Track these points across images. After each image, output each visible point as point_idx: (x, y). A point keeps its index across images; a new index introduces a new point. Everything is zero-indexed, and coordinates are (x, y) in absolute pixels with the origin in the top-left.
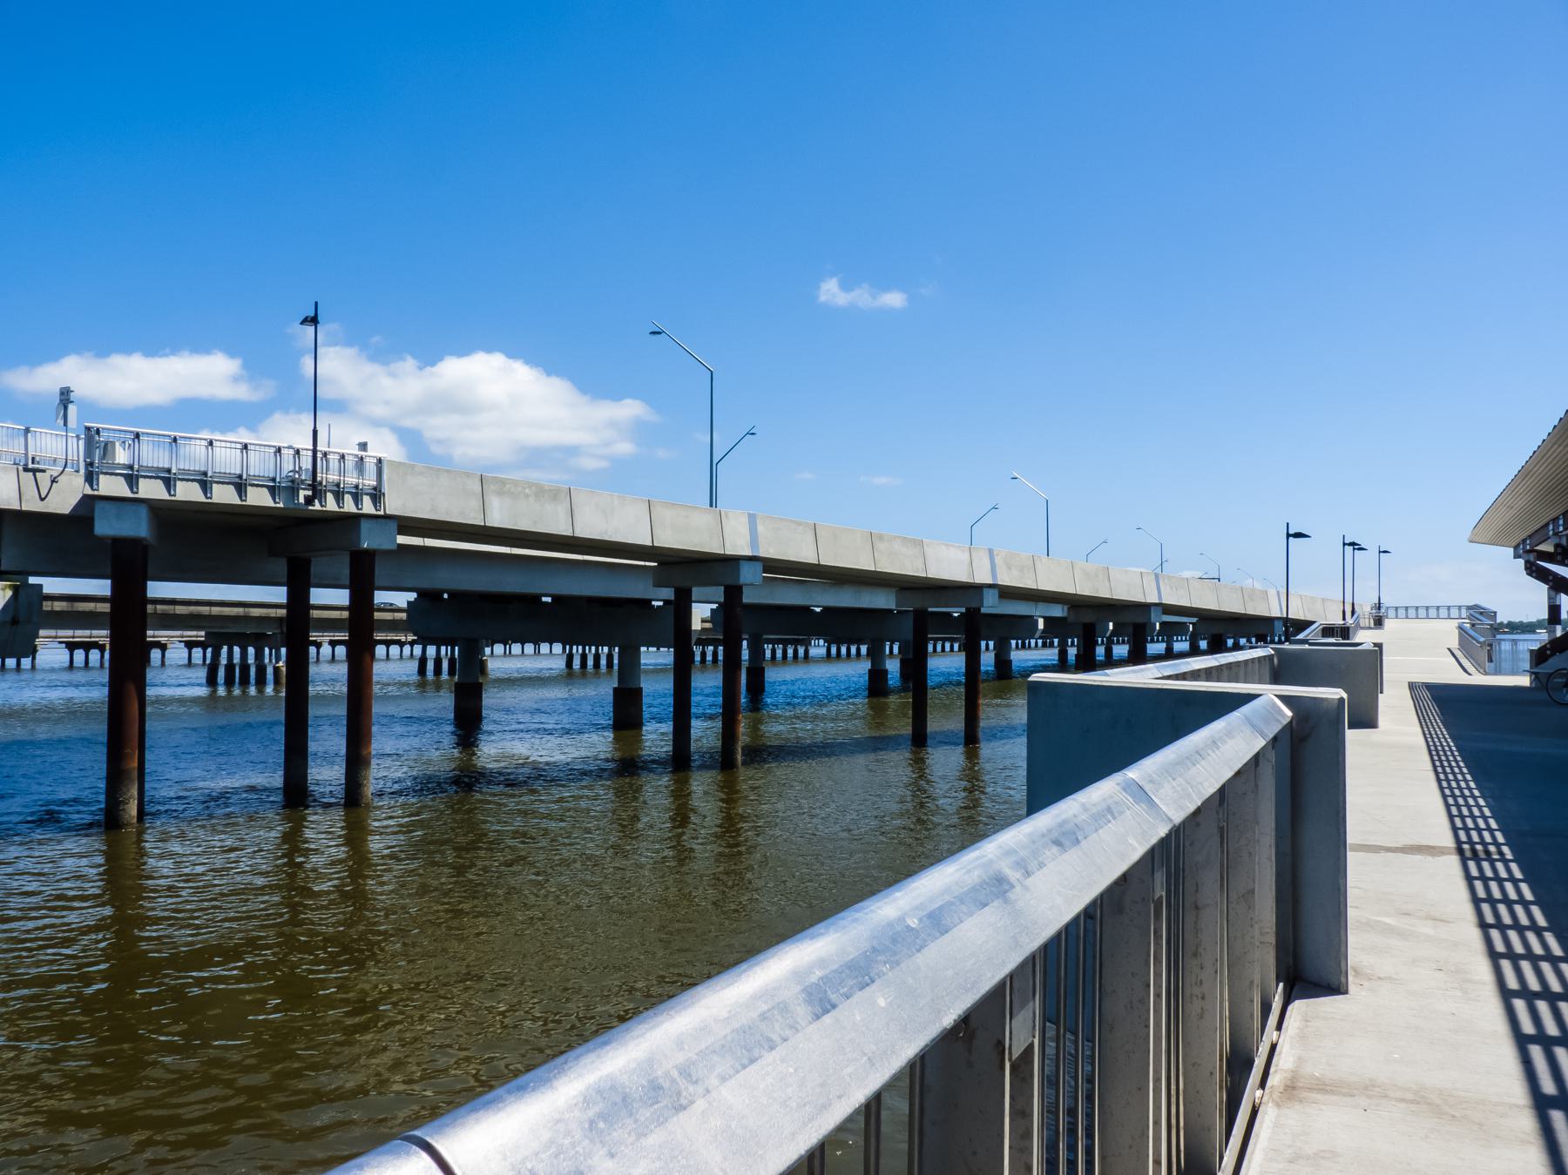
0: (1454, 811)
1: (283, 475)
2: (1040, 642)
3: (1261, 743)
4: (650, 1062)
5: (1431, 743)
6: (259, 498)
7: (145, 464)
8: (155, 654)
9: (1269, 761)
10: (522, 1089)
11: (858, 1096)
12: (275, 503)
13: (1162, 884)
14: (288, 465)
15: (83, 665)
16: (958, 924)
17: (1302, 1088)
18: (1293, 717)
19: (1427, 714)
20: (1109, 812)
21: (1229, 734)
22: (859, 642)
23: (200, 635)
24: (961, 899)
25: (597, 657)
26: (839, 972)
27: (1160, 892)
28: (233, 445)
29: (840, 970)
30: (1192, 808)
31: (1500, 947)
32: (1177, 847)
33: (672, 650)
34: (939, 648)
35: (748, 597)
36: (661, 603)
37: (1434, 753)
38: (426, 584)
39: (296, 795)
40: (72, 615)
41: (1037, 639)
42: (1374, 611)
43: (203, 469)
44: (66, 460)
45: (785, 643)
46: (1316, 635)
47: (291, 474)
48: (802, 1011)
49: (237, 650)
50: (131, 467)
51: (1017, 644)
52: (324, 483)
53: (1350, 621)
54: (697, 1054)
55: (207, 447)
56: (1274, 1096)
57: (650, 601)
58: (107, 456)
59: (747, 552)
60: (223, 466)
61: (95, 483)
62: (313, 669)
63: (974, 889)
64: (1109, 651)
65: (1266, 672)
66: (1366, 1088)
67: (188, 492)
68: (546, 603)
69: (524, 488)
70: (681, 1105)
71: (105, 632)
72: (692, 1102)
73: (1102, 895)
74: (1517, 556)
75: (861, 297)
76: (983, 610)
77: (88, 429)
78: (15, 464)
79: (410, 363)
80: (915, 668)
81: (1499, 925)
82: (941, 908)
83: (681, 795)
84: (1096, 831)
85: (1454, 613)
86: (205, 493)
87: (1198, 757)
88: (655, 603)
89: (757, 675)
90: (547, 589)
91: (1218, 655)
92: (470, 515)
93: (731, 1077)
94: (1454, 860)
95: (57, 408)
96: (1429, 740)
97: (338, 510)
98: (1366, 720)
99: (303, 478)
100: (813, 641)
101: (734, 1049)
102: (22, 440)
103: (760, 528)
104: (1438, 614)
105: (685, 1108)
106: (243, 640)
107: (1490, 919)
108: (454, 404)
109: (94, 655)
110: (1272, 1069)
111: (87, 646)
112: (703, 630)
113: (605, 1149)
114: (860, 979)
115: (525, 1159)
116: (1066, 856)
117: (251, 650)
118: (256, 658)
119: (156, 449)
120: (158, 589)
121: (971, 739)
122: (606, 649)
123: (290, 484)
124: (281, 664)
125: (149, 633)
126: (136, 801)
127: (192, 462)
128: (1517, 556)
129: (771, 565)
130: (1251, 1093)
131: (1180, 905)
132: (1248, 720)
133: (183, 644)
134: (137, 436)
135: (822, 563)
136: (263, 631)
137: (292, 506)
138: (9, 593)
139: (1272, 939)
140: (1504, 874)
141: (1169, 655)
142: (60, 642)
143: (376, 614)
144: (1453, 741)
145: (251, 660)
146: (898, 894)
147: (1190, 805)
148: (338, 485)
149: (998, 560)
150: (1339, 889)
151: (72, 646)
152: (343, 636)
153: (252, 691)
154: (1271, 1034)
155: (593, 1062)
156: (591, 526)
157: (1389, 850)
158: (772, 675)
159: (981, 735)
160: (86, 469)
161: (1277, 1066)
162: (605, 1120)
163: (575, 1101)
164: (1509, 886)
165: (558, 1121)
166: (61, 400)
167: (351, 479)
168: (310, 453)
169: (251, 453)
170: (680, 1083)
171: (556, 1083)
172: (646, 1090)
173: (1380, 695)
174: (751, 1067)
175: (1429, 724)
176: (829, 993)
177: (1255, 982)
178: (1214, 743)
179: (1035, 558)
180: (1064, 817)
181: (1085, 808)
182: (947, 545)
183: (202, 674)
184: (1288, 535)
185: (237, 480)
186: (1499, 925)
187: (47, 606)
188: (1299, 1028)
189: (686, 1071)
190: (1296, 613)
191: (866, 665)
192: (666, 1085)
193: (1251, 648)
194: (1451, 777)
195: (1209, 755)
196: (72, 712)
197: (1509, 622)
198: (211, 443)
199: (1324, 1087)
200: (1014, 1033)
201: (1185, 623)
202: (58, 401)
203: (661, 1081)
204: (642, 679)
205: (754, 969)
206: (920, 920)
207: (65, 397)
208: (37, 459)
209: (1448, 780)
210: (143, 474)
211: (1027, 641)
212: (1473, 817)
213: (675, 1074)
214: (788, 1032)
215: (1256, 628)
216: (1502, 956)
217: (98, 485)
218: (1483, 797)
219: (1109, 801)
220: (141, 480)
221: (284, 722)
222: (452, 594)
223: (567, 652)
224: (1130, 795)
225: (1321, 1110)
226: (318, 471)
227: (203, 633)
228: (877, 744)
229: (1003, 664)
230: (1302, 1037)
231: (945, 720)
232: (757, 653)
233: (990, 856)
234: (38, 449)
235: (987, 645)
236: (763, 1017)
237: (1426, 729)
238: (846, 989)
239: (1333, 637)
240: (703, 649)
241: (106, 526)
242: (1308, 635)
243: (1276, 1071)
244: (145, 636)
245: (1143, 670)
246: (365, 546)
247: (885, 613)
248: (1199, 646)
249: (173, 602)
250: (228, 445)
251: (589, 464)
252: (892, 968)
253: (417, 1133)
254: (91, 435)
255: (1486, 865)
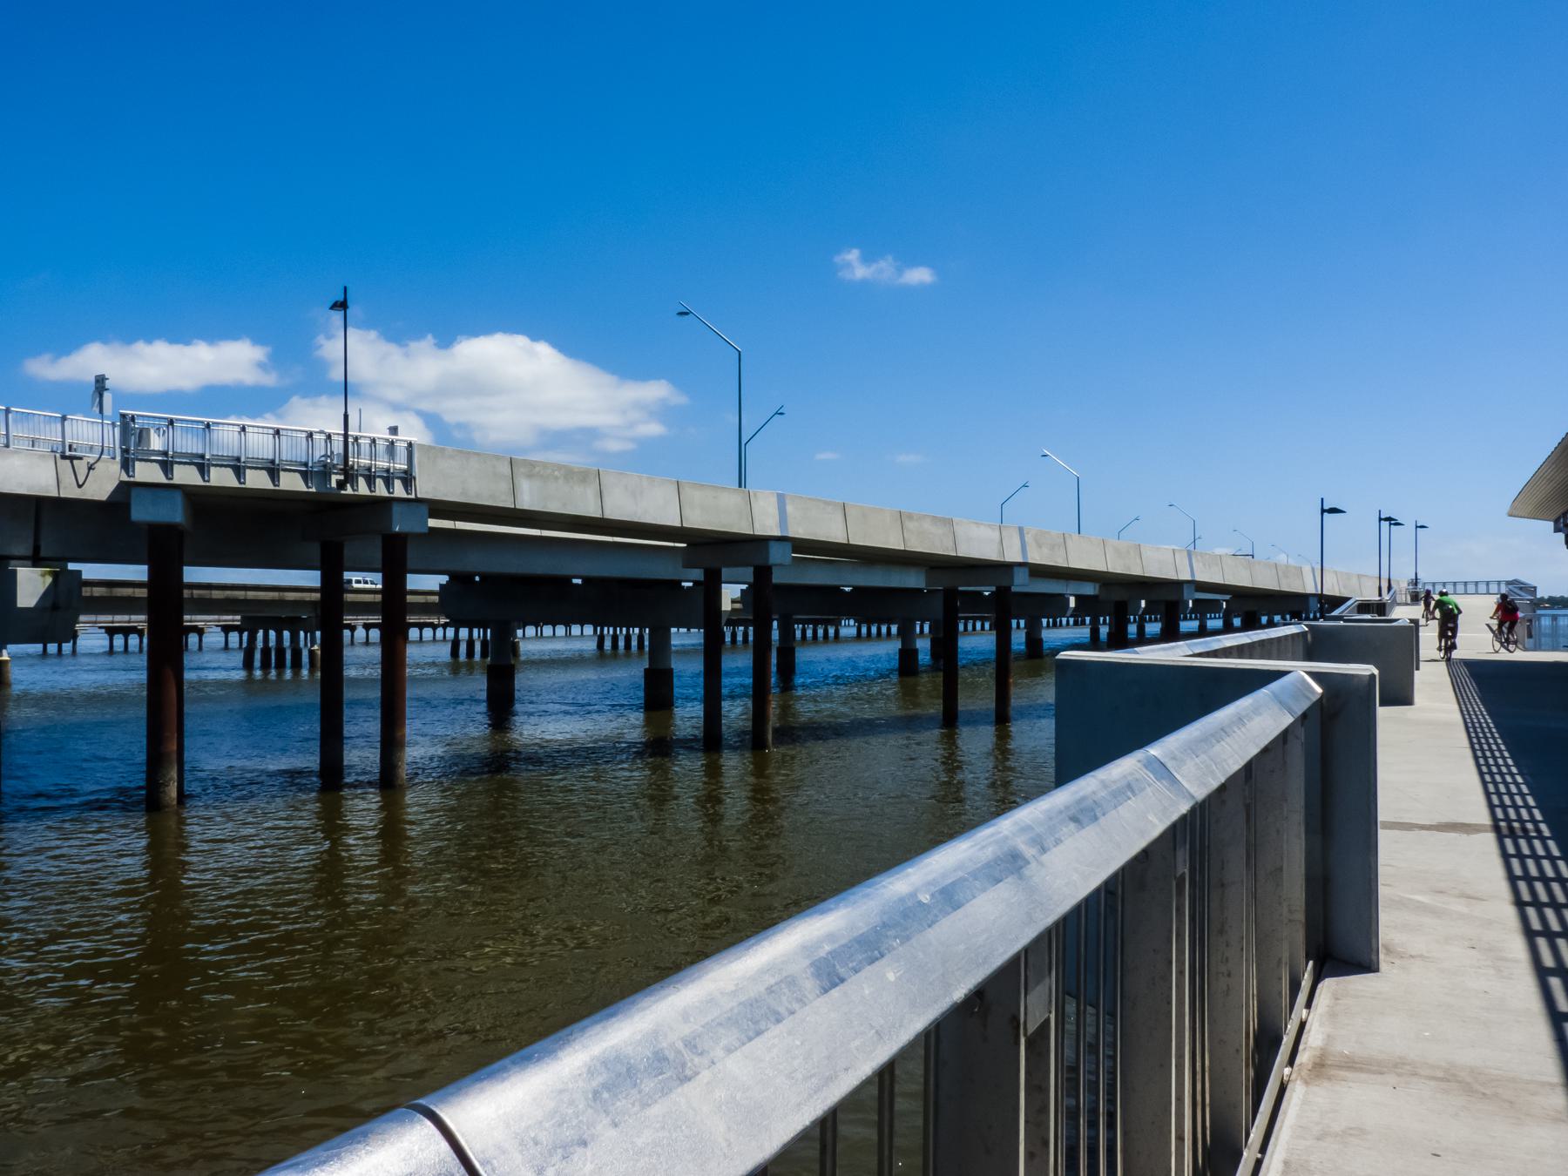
0: (1491, 788)
1: (316, 459)
2: (1071, 620)
3: (1288, 720)
4: (655, 1034)
5: (1468, 720)
6: (291, 482)
7: (179, 451)
8: (193, 639)
9: (1297, 738)
10: (528, 1059)
11: (866, 1067)
12: (308, 487)
13: (1185, 861)
14: (319, 452)
15: (122, 649)
16: (971, 900)
17: (1330, 1065)
18: (1323, 694)
19: (1464, 688)
20: (1129, 789)
21: (1256, 710)
22: (889, 622)
23: (235, 619)
24: (975, 875)
25: (628, 638)
26: (847, 946)
27: (1183, 869)
28: (265, 431)
29: (850, 945)
30: (1215, 784)
31: (1536, 925)
32: (1202, 825)
33: (702, 630)
34: (970, 627)
35: (778, 578)
36: (691, 584)
37: (1471, 730)
38: (459, 566)
39: (332, 775)
40: (111, 600)
41: (1068, 618)
42: (1411, 587)
43: (236, 455)
44: (103, 446)
45: (816, 623)
46: (1349, 612)
47: (323, 459)
48: (809, 985)
49: (272, 634)
50: (165, 453)
51: (1048, 622)
52: (356, 467)
53: (1386, 597)
54: (703, 1027)
55: (239, 432)
56: (1303, 1074)
57: (680, 581)
58: (143, 441)
59: (777, 533)
60: (265, 451)
61: (131, 470)
62: (348, 653)
63: (988, 865)
64: (1141, 629)
65: (1300, 649)
66: (1396, 1066)
67: (222, 478)
68: (577, 585)
69: (553, 471)
70: (686, 1077)
71: (143, 617)
72: (697, 1074)
73: (1123, 869)
74: (1557, 530)
75: (884, 269)
76: (1014, 589)
77: (123, 416)
78: (52, 451)
79: (426, 344)
80: (945, 646)
81: (1536, 903)
82: (953, 884)
83: (713, 771)
84: (1116, 807)
85: (1494, 588)
86: (238, 478)
87: (1223, 734)
88: (686, 584)
89: (787, 655)
90: (578, 572)
91: (1250, 633)
92: (500, 498)
93: (736, 1049)
94: (1490, 838)
95: (93, 395)
96: (1467, 717)
97: (306, 490)
98: (1400, 695)
99: (335, 462)
100: (843, 622)
101: (740, 1022)
102: (59, 426)
103: (789, 508)
104: (1477, 589)
105: (690, 1080)
106: (278, 624)
107: (1526, 897)
108: (474, 386)
109: (134, 640)
110: (1301, 1047)
111: (126, 631)
112: (733, 610)
113: (609, 1119)
114: (869, 953)
115: (528, 1128)
116: (1084, 832)
117: (286, 634)
118: (292, 642)
119: (184, 435)
120: (194, 574)
121: (1002, 718)
122: (637, 630)
123: (322, 468)
124: (316, 647)
125: (186, 617)
126: (176, 784)
127: (225, 450)
128: (1557, 530)
129: (800, 545)
130: (1280, 1069)
131: (1204, 882)
132: (1276, 696)
133: (220, 628)
134: (171, 422)
135: (851, 543)
136: (298, 615)
137: (323, 490)
138: (49, 580)
139: (1300, 916)
140: (1541, 852)
141: (1203, 632)
142: (100, 628)
143: (408, 597)
144: (1491, 718)
145: (287, 643)
146: (910, 870)
147: (1212, 782)
148: (369, 469)
149: (1028, 538)
150: (1370, 867)
151: (111, 632)
152: (376, 619)
153: (288, 674)
154: (1300, 1011)
155: (598, 1034)
156: (620, 507)
157: (1423, 827)
158: (803, 655)
159: (1012, 713)
160: (122, 456)
161: (1306, 1043)
162: (609, 1090)
163: (579, 1072)
164: (1546, 864)
165: (561, 1092)
166: (96, 388)
167: (383, 463)
168: (341, 438)
169: (283, 439)
170: (686, 1055)
171: (560, 1054)
172: (651, 1061)
173: (1416, 672)
174: (756, 1040)
175: (1472, 700)
176: (838, 967)
177: (1284, 960)
178: (1240, 720)
179: (1066, 535)
180: (1081, 794)
181: (1104, 785)
182: (976, 523)
183: (239, 658)
184: (1323, 511)
185: (403, 475)
186: (1536, 903)
187: (86, 592)
188: (1328, 1006)
189: (691, 1044)
190: (1331, 589)
191: (894, 646)
192: (671, 1056)
193: (1285, 625)
194: (1488, 754)
195: (1234, 732)
196: (114, 699)
197: (1550, 597)
198: (243, 429)
199: (1352, 1065)
200: (1029, 1008)
201: (1218, 601)
202: (94, 388)
203: (667, 1053)
204: (672, 657)
205: (763, 943)
206: (933, 895)
207: (100, 383)
208: (74, 446)
209: (1485, 758)
210: (178, 460)
211: (1058, 620)
212: (1511, 795)
213: (680, 1045)
214: (796, 1006)
215: (1291, 605)
216: (1539, 934)
217: (134, 471)
218: (1520, 773)
219: (1130, 778)
220: (176, 466)
221: (345, 706)
222: (484, 577)
223: (598, 633)
224: (1151, 772)
225: (1350, 1087)
226: (350, 455)
227: (239, 617)
228: (909, 723)
229: (1034, 642)
230: (1332, 1015)
231: (977, 698)
232: (787, 633)
233: (1006, 833)
234: (75, 437)
235: (1018, 624)
236: (770, 990)
237: (1463, 706)
238: (854, 964)
239: (1369, 613)
240: (734, 629)
241: (141, 512)
242: (1343, 612)
243: (1305, 1049)
244: (182, 621)
245: (1173, 648)
246: (397, 529)
247: (915, 592)
248: (1233, 624)
249: (209, 587)
250: (261, 430)
251: (614, 446)
252: (902, 943)
253: (422, 1101)
254: (126, 422)
255: (1523, 842)
